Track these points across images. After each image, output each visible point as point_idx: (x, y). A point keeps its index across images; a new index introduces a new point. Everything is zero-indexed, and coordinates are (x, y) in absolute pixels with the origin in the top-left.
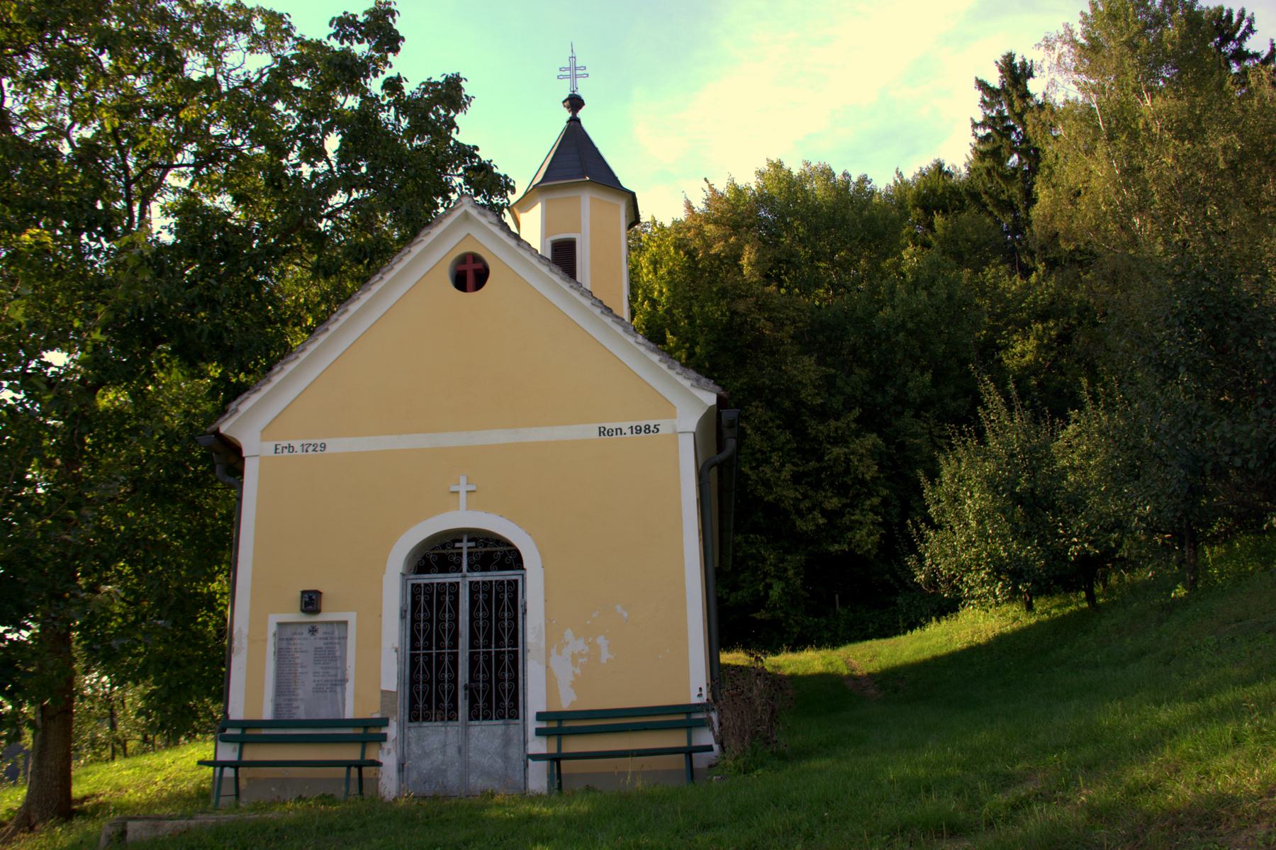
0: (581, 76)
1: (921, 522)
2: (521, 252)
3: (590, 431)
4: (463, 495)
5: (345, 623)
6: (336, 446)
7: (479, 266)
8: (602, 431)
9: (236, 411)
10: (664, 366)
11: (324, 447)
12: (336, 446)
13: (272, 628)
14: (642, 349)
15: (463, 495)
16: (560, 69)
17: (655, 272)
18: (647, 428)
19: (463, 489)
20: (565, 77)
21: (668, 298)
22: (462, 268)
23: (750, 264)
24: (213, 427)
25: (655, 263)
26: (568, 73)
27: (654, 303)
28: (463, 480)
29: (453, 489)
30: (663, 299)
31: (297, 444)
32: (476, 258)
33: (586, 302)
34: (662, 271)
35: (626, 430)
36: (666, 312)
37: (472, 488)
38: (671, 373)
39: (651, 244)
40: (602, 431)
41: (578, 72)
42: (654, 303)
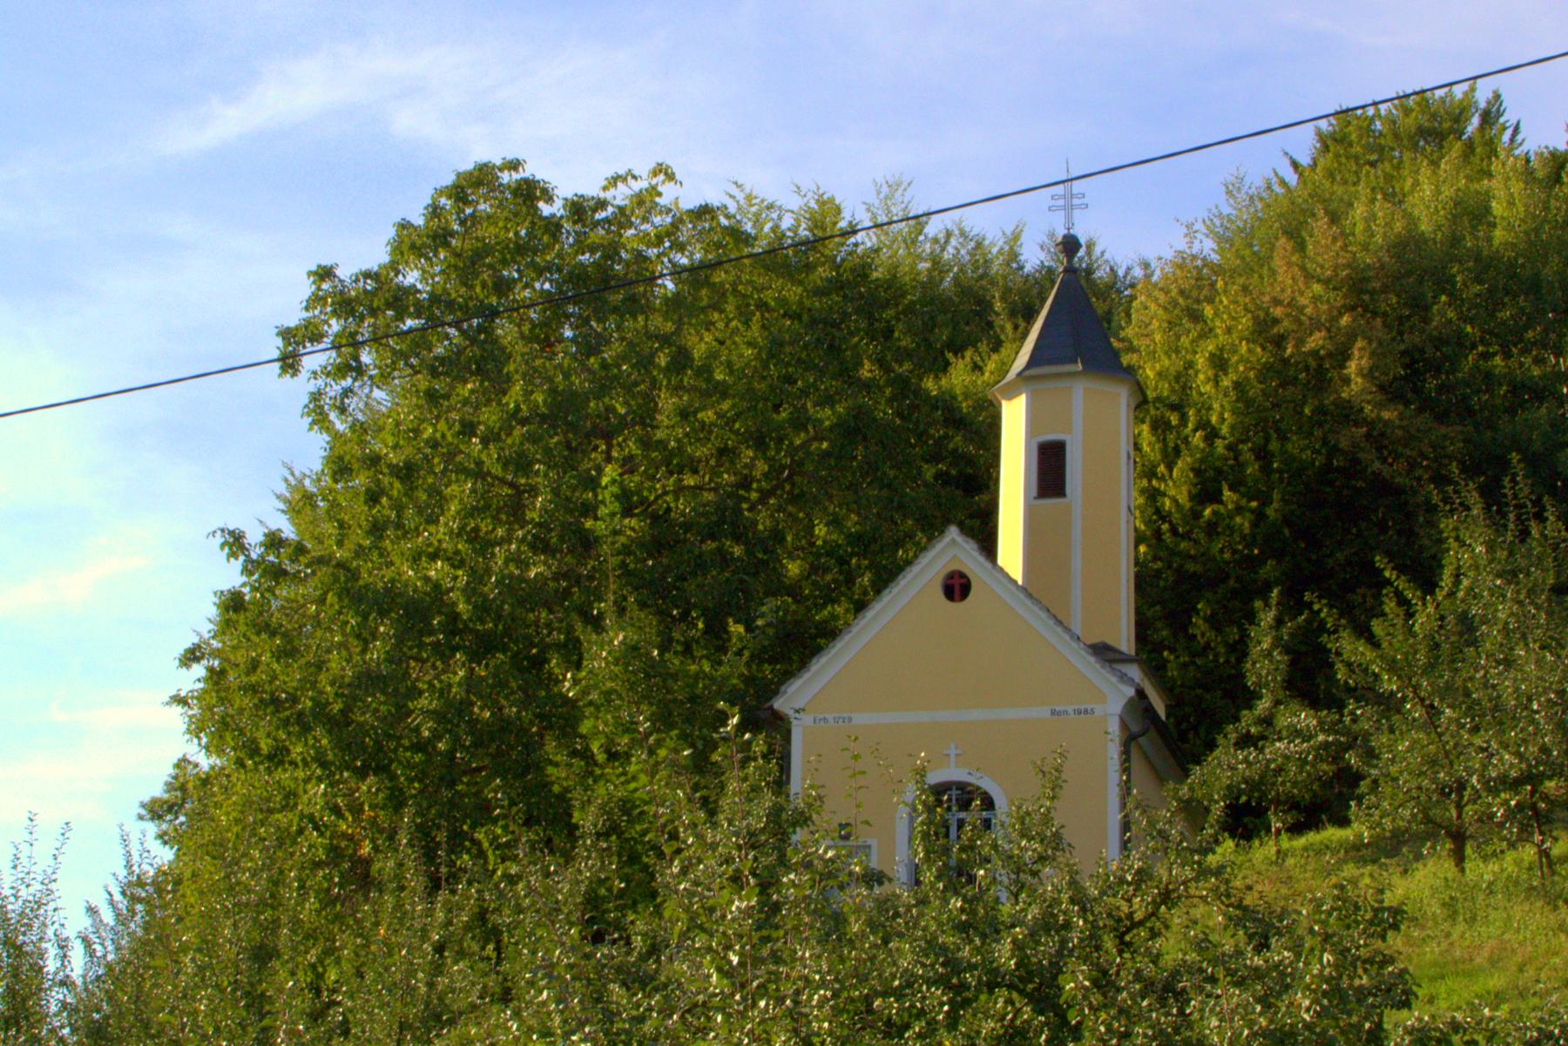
0: (1079, 207)
1: (186, 815)
2: (995, 573)
3: (1044, 712)
4: (953, 758)
5: (869, 847)
6: (860, 719)
7: (964, 581)
8: (1053, 713)
9: (785, 692)
10: (1098, 666)
11: (850, 720)
12: (860, 719)
13: (987, 785)
14: (1083, 653)
15: (953, 758)
16: (1052, 198)
17: (1217, 383)
18: (1086, 711)
19: (953, 752)
20: (1058, 208)
21: (1233, 427)
22: (950, 582)
23: (1360, 372)
24: (768, 704)
25: (1219, 363)
26: (1061, 202)
27: (1212, 435)
28: (952, 746)
29: (946, 752)
30: (1225, 430)
31: (830, 717)
32: (962, 575)
33: (1043, 615)
34: (1226, 382)
35: (1070, 711)
36: (1230, 448)
37: (958, 752)
38: (1104, 672)
39: (1218, 323)
40: (1053, 713)
41: (1076, 201)
42: (1212, 435)
